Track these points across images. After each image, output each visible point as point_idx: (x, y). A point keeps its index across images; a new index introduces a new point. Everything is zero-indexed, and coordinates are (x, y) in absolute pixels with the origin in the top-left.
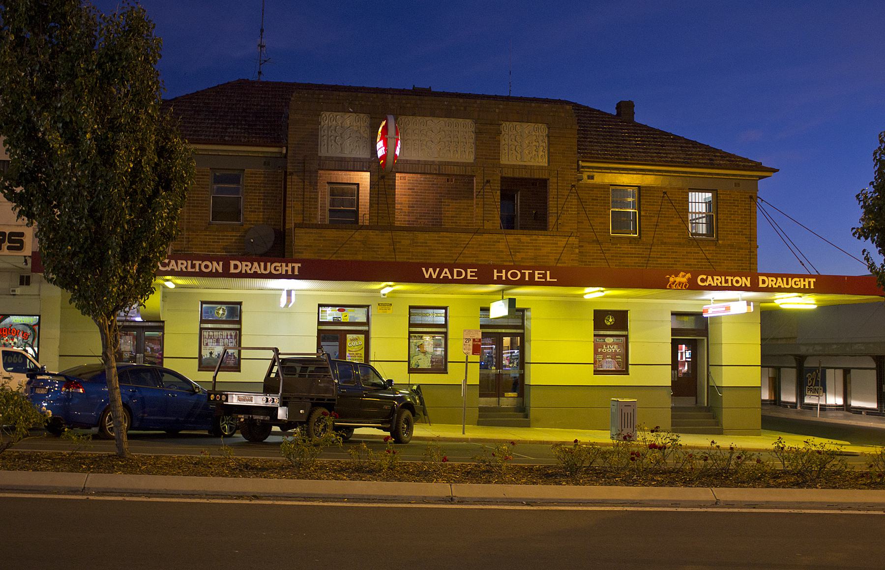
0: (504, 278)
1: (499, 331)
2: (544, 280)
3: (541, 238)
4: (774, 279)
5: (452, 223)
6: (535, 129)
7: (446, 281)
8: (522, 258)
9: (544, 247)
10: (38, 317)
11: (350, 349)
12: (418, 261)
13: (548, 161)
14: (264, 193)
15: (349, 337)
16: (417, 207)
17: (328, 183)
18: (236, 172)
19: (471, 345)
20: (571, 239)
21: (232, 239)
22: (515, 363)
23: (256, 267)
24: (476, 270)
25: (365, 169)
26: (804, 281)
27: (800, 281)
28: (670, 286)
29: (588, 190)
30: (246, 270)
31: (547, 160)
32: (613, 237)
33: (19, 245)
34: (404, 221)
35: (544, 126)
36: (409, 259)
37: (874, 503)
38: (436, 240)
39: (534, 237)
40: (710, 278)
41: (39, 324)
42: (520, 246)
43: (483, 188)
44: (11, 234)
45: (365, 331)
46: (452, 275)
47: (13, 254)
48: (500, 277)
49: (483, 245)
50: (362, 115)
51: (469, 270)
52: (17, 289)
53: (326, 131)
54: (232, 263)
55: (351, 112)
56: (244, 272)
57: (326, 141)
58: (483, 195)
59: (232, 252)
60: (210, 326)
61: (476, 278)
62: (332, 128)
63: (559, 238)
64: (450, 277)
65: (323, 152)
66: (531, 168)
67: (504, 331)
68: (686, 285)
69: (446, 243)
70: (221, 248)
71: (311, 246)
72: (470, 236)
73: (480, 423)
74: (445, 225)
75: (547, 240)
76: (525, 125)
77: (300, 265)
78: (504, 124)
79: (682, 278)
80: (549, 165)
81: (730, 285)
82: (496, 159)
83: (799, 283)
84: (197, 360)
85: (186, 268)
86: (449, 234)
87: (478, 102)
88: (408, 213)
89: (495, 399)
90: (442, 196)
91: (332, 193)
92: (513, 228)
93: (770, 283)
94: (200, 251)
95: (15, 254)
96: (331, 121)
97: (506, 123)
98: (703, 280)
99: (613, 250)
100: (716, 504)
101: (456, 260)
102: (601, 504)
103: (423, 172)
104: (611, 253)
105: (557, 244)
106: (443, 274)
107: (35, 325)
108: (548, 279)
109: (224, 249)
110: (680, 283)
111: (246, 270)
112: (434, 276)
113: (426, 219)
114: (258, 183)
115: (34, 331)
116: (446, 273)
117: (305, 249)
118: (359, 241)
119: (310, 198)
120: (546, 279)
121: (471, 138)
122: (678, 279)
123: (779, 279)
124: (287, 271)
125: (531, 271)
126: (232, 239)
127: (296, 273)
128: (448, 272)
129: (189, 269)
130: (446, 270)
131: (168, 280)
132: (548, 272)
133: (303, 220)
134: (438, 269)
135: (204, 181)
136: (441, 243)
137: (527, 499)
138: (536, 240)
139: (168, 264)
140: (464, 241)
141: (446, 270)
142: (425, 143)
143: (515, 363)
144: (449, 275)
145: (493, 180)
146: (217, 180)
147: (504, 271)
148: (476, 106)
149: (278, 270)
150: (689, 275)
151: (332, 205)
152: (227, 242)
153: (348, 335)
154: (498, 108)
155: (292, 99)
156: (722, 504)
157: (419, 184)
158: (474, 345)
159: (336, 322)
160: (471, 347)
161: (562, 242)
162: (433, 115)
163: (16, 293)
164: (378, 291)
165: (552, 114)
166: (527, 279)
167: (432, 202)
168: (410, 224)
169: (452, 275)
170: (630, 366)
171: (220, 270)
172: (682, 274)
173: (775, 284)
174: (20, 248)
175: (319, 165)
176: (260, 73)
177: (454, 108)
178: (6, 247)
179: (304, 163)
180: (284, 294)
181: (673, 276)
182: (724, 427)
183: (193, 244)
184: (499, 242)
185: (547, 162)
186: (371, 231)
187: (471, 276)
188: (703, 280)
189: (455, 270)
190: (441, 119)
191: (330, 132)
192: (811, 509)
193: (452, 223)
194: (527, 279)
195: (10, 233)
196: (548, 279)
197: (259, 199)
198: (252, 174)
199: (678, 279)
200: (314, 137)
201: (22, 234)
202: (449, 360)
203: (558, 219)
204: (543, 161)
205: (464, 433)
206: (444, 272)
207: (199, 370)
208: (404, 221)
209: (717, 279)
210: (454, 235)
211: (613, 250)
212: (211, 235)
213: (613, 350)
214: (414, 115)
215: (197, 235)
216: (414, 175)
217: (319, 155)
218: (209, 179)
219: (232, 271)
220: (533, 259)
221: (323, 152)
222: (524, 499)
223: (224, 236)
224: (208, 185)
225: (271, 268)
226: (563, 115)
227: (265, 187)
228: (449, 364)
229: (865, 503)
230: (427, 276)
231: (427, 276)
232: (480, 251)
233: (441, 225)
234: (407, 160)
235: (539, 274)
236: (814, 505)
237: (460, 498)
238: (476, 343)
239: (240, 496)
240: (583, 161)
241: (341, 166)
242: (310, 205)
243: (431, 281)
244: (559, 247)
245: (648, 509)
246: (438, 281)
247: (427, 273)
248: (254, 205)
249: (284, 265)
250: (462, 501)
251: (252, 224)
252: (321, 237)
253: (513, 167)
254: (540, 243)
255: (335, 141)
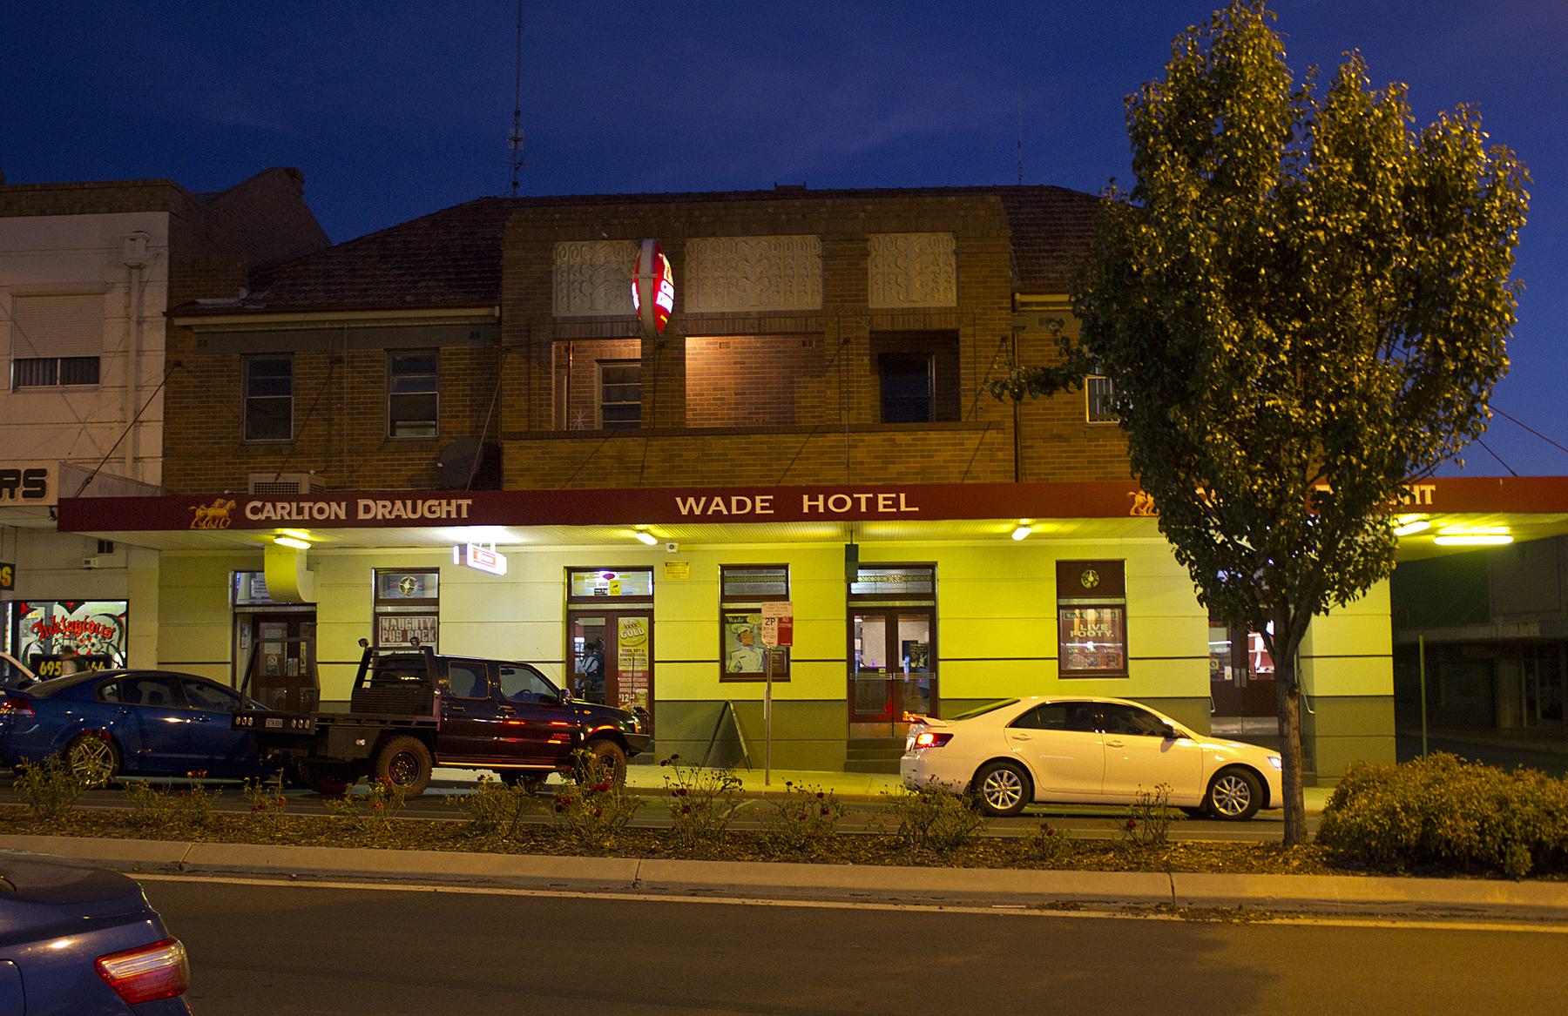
0: (821, 510)
1: (890, 604)
2: (895, 510)
3: (933, 435)
4: (388, 504)
5: (812, 417)
6: (932, 243)
7: (718, 518)
8: (898, 473)
9: (940, 451)
10: (125, 603)
11: (624, 642)
12: (713, 486)
13: (958, 298)
14: (472, 385)
15: (623, 621)
16: (750, 394)
17: (597, 361)
18: (282, 358)
19: (776, 628)
20: (988, 434)
21: (421, 464)
22: (922, 660)
23: (400, 509)
24: (771, 497)
25: (631, 335)
26: (449, 504)
27: (440, 504)
28: (1136, 511)
29: (1041, 346)
30: (383, 515)
31: (955, 294)
32: (1091, 428)
33: (39, 489)
34: (729, 419)
35: (947, 236)
36: (697, 483)
37: (947, 892)
38: (744, 449)
39: (920, 434)
40: (269, 506)
41: (126, 614)
42: (894, 451)
43: (838, 354)
44: (29, 472)
45: (649, 610)
46: (729, 508)
47: (30, 504)
48: (813, 508)
49: (827, 453)
50: (626, 242)
51: (758, 499)
52: (92, 560)
53: (565, 275)
54: (362, 503)
55: (604, 239)
56: (380, 517)
57: (565, 291)
58: (838, 366)
59: (421, 486)
60: (390, 609)
61: (772, 512)
62: (574, 269)
63: (966, 434)
64: (725, 512)
65: (561, 310)
66: (925, 312)
67: (898, 604)
68: (226, 521)
69: (761, 454)
70: (404, 481)
71: (529, 470)
72: (803, 438)
73: (849, 768)
74: (800, 422)
75: (944, 439)
76: (913, 237)
77: (1433, 488)
78: (874, 239)
79: (219, 510)
80: (958, 304)
81: (307, 517)
82: (859, 301)
83: (438, 509)
84: (718, 664)
85: (289, 514)
86: (764, 438)
87: (829, 202)
88: (735, 404)
89: (886, 726)
90: (794, 372)
91: (607, 377)
92: (926, 420)
93: (381, 510)
94: (371, 487)
95: (36, 504)
96: (570, 255)
97: (878, 235)
98: (255, 511)
99: (1090, 451)
100: (634, 886)
101: (780, 481)
102: (425, 882)
103: (731, 332)
104: (1087, 457)
105: (962, 444)
106: (713, 508)
107: (121, 616)
108: (903, 508)
109: (408, 480)
110: (214, 519)
111: (383, 515)
112: (697, 512)
113: (767, 413)
114: (461, 369)
115: (120, 625)
116: (717, 505)
117: (521, 476)
118: (610, 457)
119: (540, 389)
120: (898, 508)
121: (948, 266)
122: (212, 512)
123: (399, 504)
124: (449, 513)
125: (871, 495)
126: (421, 464)
127: (464, 515)
128: (721, 503)
129: (294, 517)
130: (718, 499)
131: (279, 536)
132: (902, 496)
133: (529, 427)
134: (704, 499)
135: (375, 372)
136: (751, 454)
137: (298, 869)
138: (925, 439)
139: (261, 510)
140: (794, 448)
141: (718, 499)
142: (734, 281)
143: (922, 660)
144: (722, 508)
145: (857, 338)
146: (398, 368)
147: (821, 497)
148: (823, 210)
149: (435, 512)
150: (232, 504)
151: (607, 395)
152: (412, 470)
153: (620, 619)
154: (864, 211)
155: (508, 224)
156: (644, 887)
157: (753, 353)
158: (780, 629)
159: (601, 597)
160: (776, 633)
161: (972, 440)
162: (747, 232)
163: (92, 565)
164: (1008, 536)
165: (962, 213)
166: (863, 509)
167: (777, 383)
168: (740, 423)
169: (729, 508)
170: (1130, 661)
171: (343, 517)
172: (219, 501)
173: (390, 513)
174: (41, 494)
175: (554, 332)
176: (515, 184)
177: (784, 217)
178: (21, 493)
179: (529, 331)
180: (456, 550)
181: (203, 507)
182: (1319, 773)
183: (358, 476)
184: (856, 446)
185: (955, 300)
186: (630, 439)
187: (763, 508)
188: (255, 511)
189: (734, 499)
190: (761, 238)
191: (571, 276)
192: (799, 899)
193: (812, 417)
194: (863, 509)
195: (27, 471)
196: (903, 508)
197: (463, 395)
198: (450, 354)
199: (212, 512)
200: (544, 285)
201: (43, 472)
202: (1130, 655)
203: (977, 400)
204: (944, 296)
205: (767, 784)
206: (714, 503)
207: (721, 681)
208: (729, 419)
209: (283, 508)
210: (774, 438)
211: (1090, 451)
212: (387, 460)
213: (1100, 633)
214: (714, 234)
215: (366, 460)
216: (742, 338)
217: (554, 315)
218: (383, 366)
219: (362, 516)
220: (919, 473)
221: (561, 310)
222: (294, 870)
223: (410, 459)
224: (381, 377)
225: (423, 509)
226: (982, 213)
227: (473, 374)
228: (718, 658)
229: (926, 892)
230: (685, 512)
231: (685, 512)
232: (823, 464)
233: (794, 422)
234: (702, 314)
235: (885, 499)
236: (820, 893)
237: (194, 865)
238: (784, 625)
239: (240, 872)
240: (1022, 293)
241: (591, 331)
242: (540, 400)
243: (691, 519)
244: (968, 450)
245: (514, 892)
246: (703, 519)
247: (685, 506)
248: (455, 406)
249: (444, 502)
250: (194, 871)
251: (453, 438)
252: (547, 453)
253: (892, 313)
254: (931, 445)
255: (580, 290)
